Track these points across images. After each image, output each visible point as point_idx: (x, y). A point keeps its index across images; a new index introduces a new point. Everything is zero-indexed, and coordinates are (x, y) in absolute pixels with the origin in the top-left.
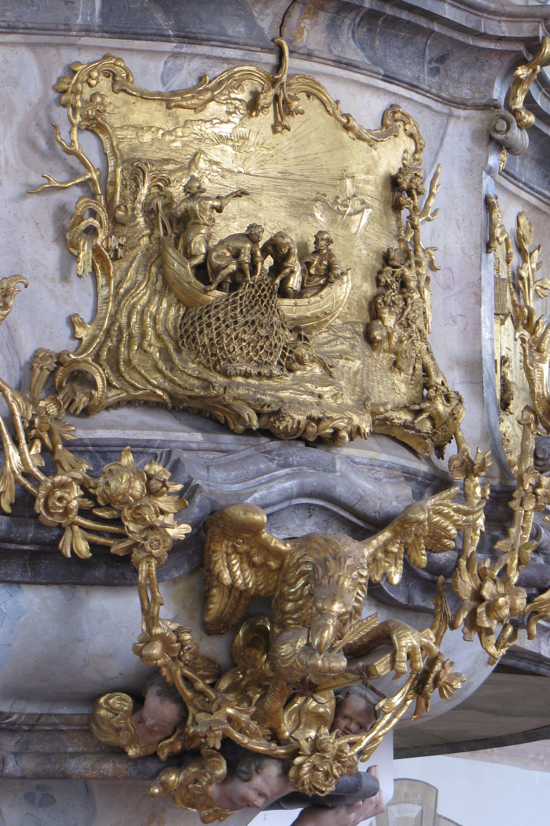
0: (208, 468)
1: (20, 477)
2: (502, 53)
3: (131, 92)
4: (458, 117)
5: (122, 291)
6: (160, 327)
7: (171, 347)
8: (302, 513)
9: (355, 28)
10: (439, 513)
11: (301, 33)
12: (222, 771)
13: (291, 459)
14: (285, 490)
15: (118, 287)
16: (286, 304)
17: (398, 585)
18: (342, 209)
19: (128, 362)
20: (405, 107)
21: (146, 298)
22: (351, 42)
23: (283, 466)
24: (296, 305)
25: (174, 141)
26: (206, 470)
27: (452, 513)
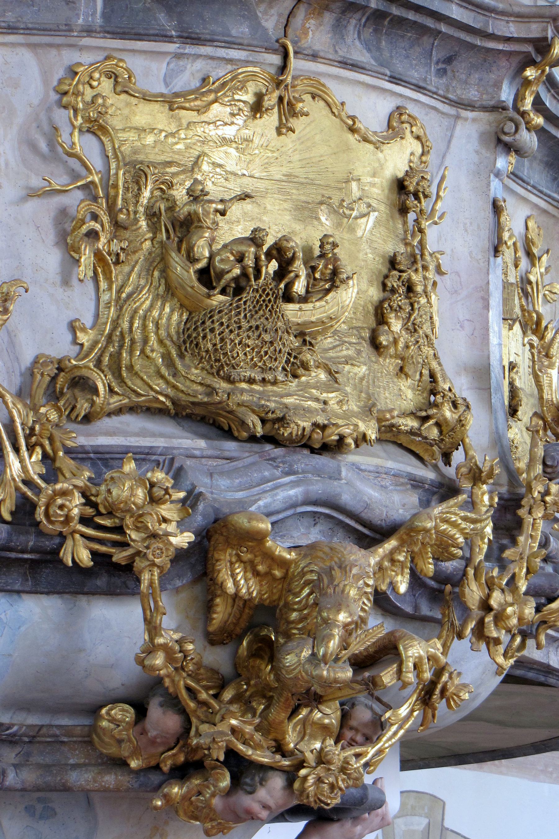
0: (211, 475)
1: (21, 485)
2: (510, 54)
3: (133, 93)
4: (466, 119)
5: (124, 295)
6: (162, 333)
7: (174, 353)
8: (307, 521)
9: (361, 28)
10: (446, 521)
11: (306, 34)
12: (225, 782)
13: (296, 466)
14: (290, 497)
15: (120, 291)
16: (290, 309)
17: (405, 594)
18: (347, 212)
19: (130, 368)
20: (412, 109)
21: (148, 303)
22: (357, 42)
23: (288, 474)
24: (300, 309)
25: (176, 143)
26: (209, 478)
27: (460, 521)
